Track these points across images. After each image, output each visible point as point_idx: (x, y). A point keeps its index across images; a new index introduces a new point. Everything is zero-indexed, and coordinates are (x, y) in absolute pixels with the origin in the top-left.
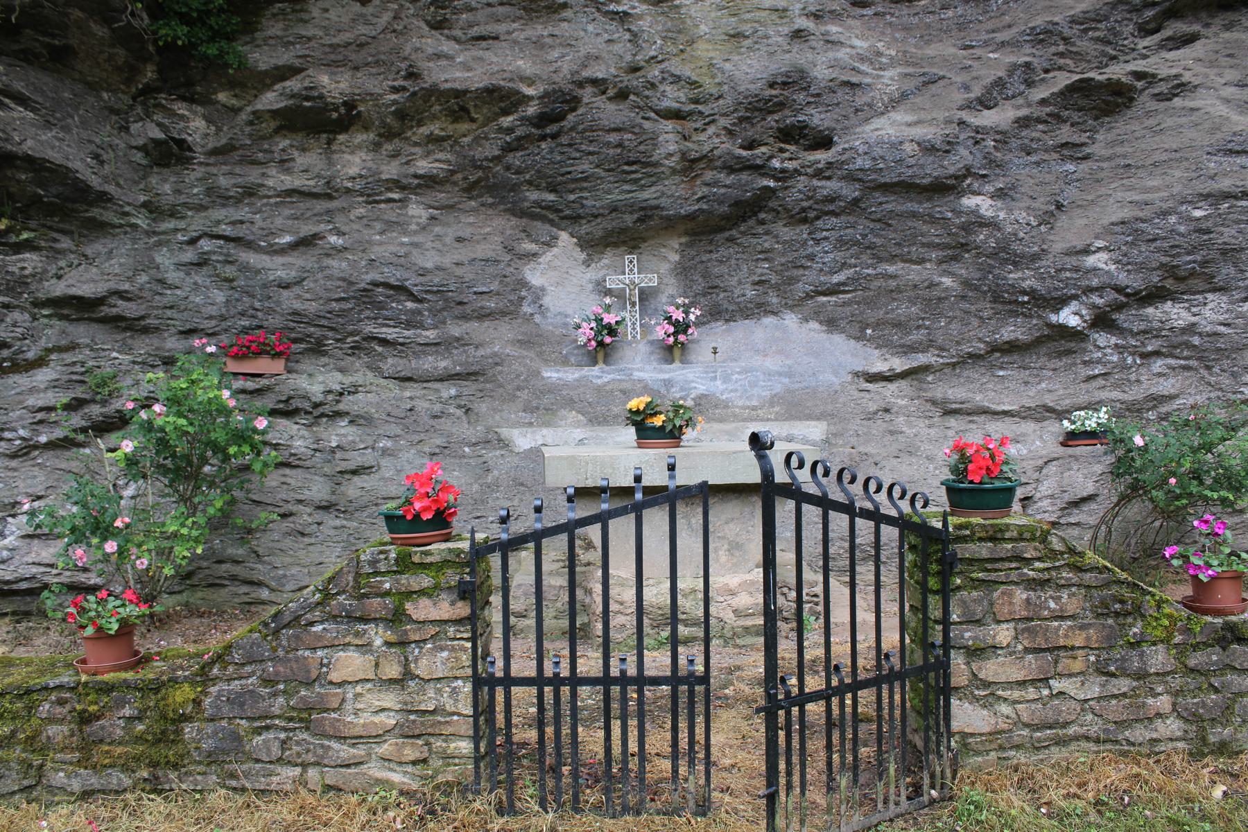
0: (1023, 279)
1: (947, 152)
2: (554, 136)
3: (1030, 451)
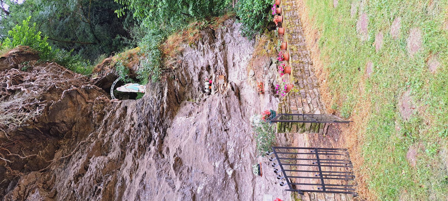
0: (220, 182)
1: (185, 195)
3: (263, 183)
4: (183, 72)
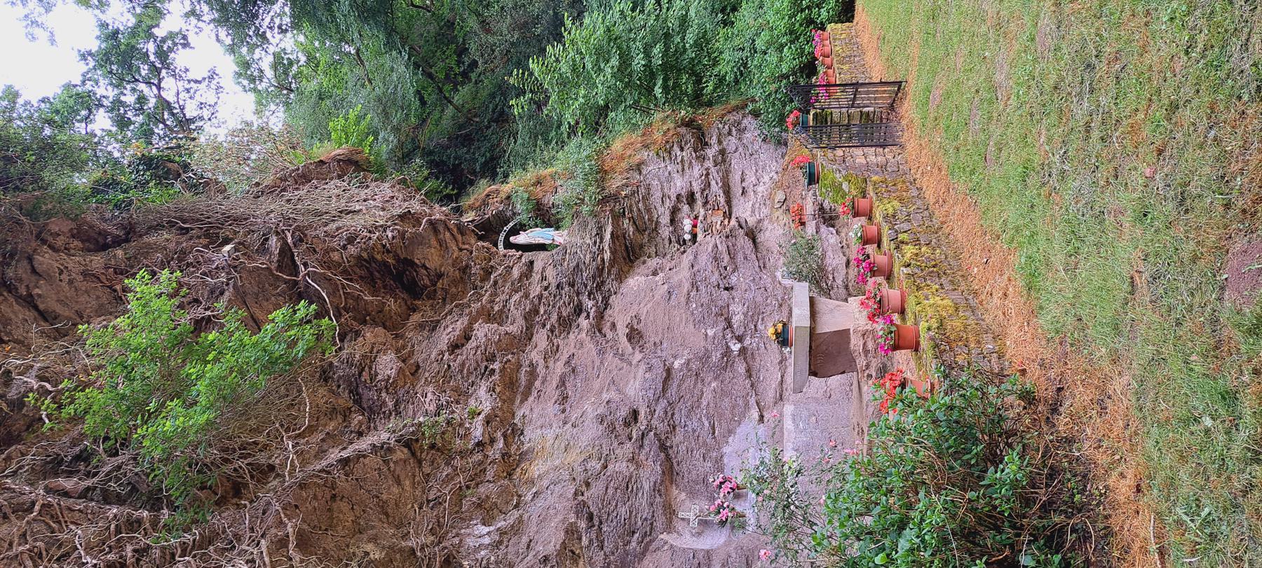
2: (601, 523)
4: (640, 205)
